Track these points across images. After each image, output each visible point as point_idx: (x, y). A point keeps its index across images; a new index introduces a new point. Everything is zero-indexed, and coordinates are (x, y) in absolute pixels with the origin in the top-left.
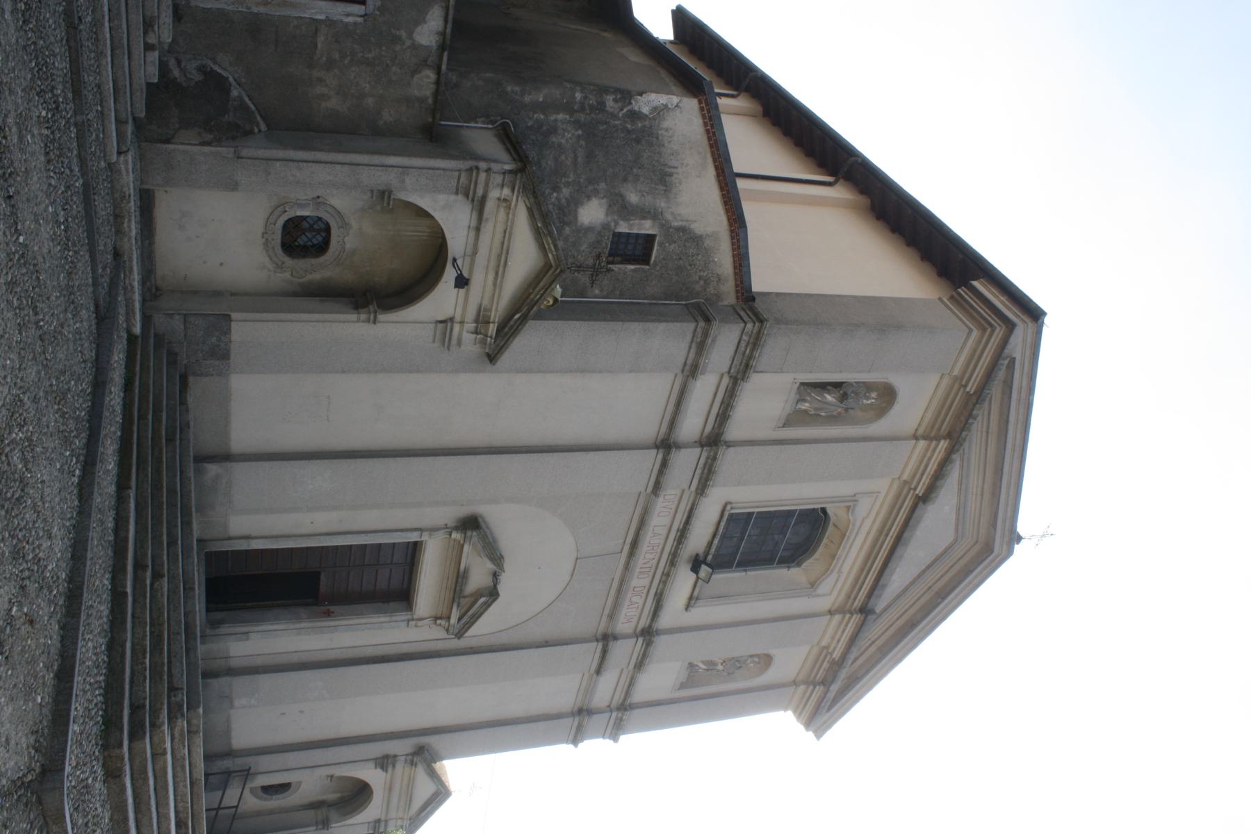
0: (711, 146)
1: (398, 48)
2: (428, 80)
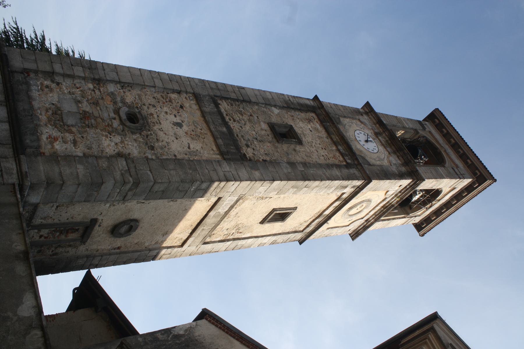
0: (227, 333)
1: (9, 323)
2: (37, 337)
